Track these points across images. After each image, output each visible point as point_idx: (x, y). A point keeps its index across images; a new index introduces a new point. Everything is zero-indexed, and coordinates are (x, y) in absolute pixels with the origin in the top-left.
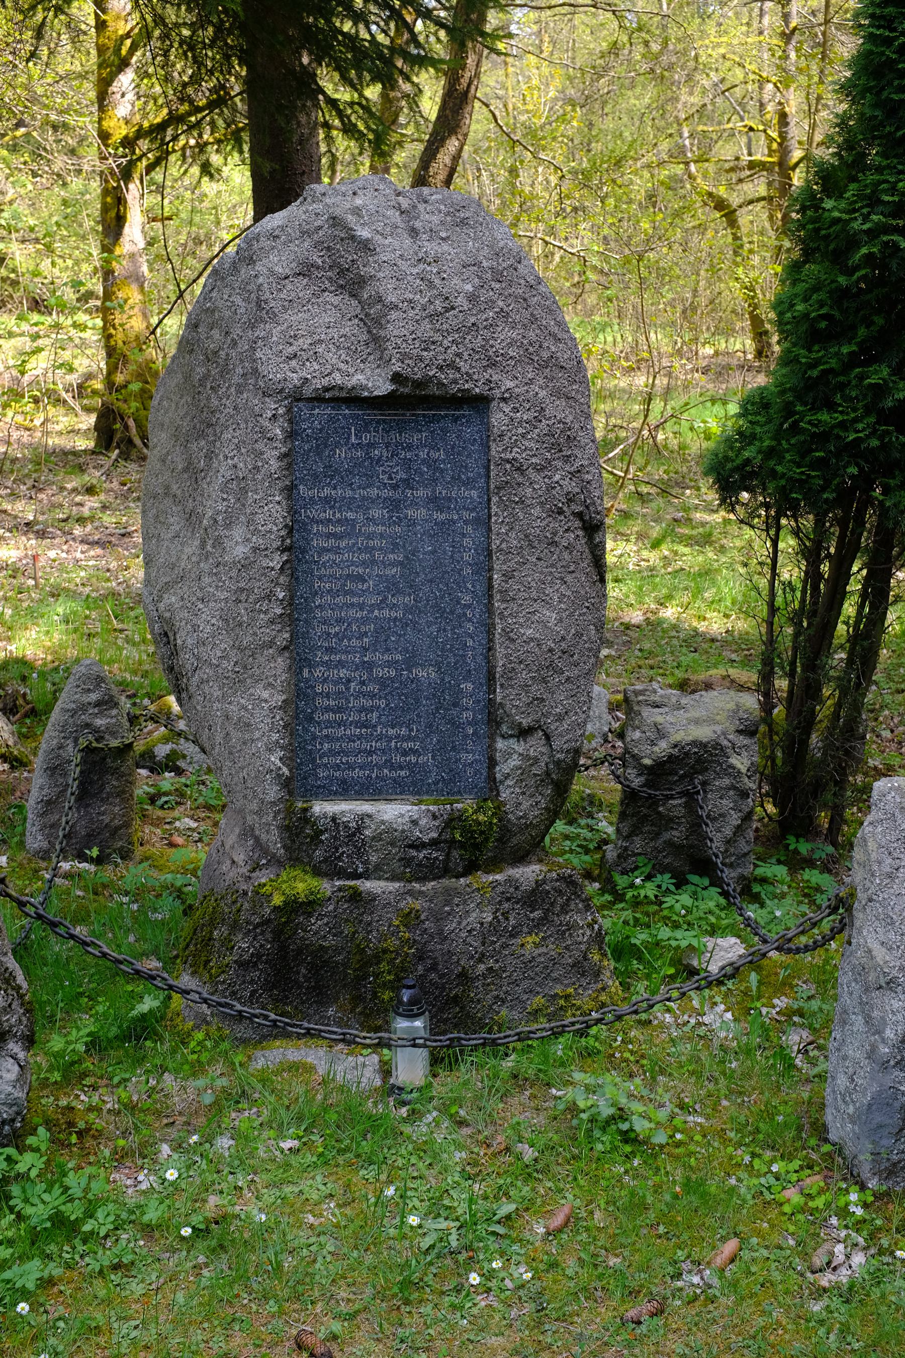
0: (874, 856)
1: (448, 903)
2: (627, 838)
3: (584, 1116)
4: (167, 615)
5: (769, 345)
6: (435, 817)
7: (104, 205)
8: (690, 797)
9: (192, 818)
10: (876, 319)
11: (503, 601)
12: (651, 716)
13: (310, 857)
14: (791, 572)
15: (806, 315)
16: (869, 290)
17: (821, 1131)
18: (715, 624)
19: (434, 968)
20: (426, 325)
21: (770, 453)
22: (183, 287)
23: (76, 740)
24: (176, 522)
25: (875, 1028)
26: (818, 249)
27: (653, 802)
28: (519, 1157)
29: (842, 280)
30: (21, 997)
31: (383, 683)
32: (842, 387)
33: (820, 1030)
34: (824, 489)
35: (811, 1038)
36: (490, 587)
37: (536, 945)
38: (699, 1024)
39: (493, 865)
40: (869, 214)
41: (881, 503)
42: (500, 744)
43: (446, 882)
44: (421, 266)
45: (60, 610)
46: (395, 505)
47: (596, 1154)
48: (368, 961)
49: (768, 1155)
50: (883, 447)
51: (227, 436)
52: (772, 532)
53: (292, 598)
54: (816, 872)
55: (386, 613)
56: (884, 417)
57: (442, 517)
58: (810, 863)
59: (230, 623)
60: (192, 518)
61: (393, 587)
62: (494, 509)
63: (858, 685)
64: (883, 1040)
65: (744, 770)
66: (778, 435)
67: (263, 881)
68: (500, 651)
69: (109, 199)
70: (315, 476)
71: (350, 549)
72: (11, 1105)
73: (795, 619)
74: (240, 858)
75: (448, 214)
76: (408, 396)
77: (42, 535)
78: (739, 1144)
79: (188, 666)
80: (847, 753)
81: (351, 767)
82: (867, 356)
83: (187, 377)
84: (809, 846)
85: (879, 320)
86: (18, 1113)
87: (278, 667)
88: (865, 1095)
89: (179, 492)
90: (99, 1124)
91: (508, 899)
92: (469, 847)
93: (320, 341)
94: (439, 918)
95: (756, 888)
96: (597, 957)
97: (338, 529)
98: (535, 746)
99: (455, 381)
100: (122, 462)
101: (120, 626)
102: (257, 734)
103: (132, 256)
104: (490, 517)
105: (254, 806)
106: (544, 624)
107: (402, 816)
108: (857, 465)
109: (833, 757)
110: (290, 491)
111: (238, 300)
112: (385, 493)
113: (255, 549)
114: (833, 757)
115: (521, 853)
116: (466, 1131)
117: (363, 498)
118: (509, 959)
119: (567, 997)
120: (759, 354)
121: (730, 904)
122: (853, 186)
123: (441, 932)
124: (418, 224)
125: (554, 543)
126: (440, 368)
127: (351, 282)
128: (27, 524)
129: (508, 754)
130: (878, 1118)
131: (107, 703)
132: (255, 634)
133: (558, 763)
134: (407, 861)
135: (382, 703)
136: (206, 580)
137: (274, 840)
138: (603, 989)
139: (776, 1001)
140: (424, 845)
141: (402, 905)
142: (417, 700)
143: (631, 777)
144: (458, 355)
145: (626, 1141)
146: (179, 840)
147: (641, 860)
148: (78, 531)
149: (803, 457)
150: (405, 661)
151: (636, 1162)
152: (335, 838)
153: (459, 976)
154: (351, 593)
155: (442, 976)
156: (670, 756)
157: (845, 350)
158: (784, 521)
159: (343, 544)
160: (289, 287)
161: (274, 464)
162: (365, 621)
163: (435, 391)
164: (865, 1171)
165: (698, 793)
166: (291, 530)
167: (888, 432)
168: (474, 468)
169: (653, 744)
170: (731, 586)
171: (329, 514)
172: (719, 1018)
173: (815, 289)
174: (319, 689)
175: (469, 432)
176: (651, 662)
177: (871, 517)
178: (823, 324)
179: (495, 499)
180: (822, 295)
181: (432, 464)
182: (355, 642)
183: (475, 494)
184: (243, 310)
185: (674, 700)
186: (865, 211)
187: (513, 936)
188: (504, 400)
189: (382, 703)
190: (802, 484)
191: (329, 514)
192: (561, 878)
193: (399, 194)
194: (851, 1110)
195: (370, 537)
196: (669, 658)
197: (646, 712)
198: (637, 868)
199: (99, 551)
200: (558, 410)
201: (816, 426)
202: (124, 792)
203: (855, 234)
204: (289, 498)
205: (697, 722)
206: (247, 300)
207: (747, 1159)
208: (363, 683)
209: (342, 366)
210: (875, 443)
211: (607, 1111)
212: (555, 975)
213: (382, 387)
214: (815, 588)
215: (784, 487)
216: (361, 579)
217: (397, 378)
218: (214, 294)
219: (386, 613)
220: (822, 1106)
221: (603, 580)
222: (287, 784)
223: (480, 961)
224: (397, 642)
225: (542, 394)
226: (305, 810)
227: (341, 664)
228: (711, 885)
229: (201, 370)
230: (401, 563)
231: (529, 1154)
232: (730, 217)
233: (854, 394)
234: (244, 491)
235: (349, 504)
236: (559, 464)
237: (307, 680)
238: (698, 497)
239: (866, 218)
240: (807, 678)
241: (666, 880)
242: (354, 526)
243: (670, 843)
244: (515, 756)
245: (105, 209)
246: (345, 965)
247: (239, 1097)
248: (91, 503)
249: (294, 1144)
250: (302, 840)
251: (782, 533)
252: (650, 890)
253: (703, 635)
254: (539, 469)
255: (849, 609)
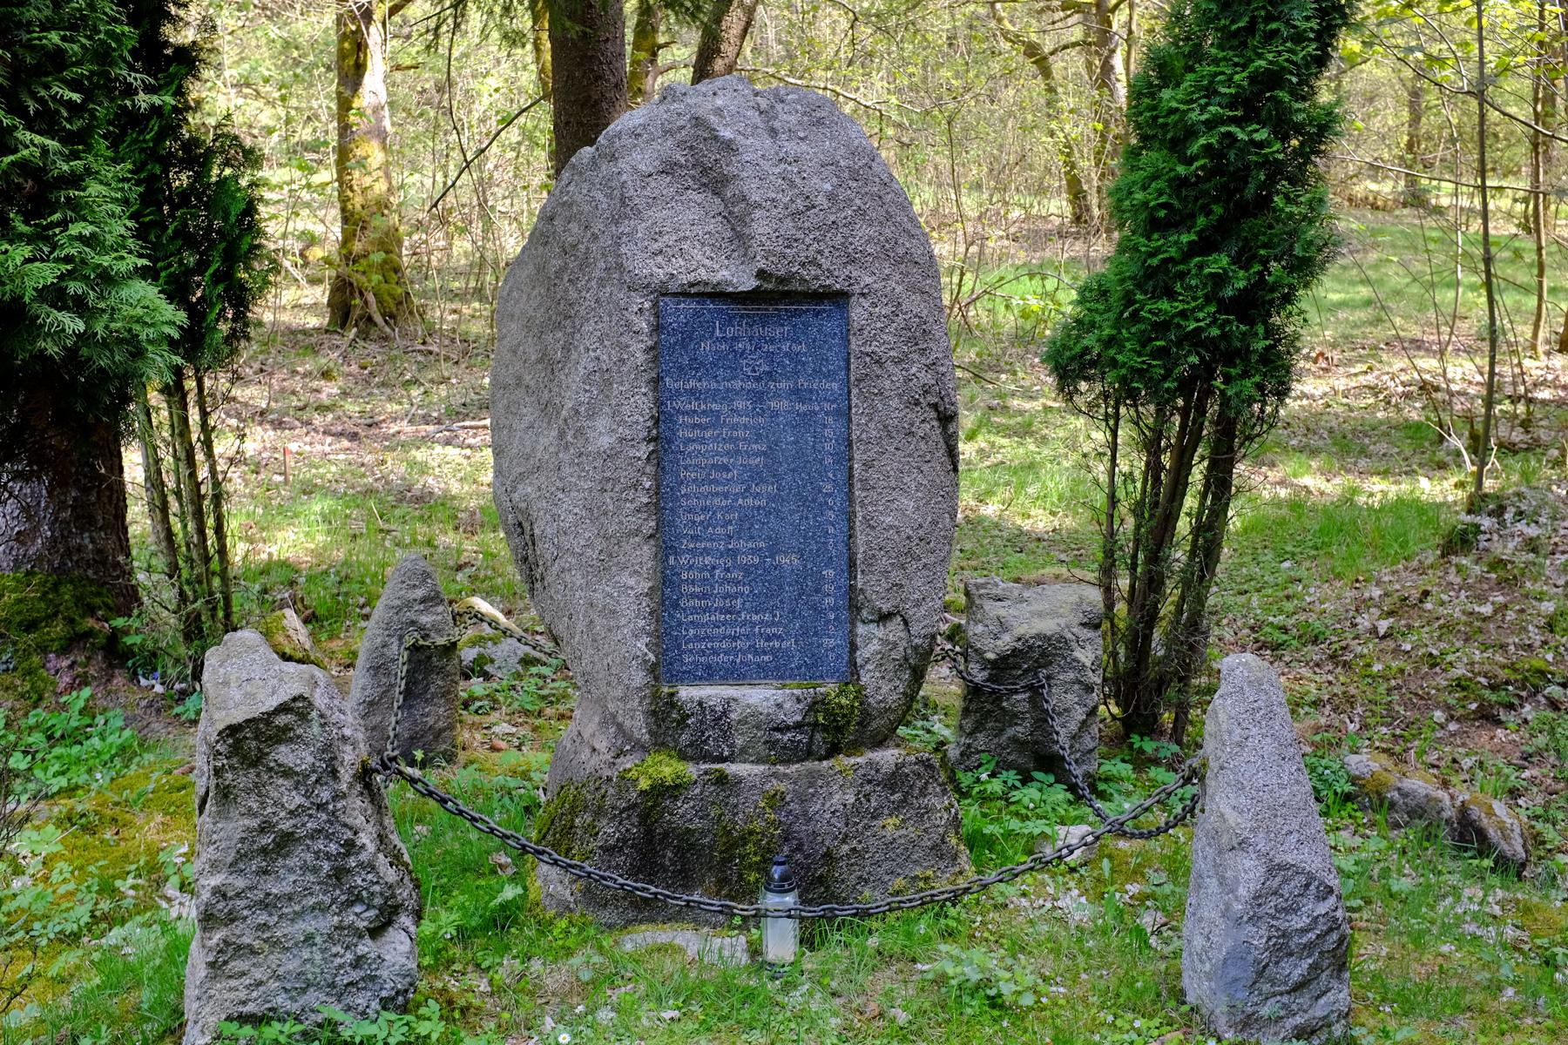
0: (1224, 726)
1: (811, 785)
2: (970, 735)
3: (954, 982)
4: (523, 505)
5: (1088, 209)
6: (799, 700)
7: (341, 51)
8: (1035, 691)
9: (509, 722)
10: (1214, 207)
11: (864, 490)
12: (993, 609)
13: (675, 741)
14: (1132, 462)
15: (1145, 204)
16: (1207, 179)
17: (1180, 996)
18: (1041, 521)
19: (799, 848)
20: (788, 223)
21: (1110, 342)
22: (469, 157)
23: (401, 638)
24: (529, 413)
25: (1228, 886)
26: (1155, 136)
27: (997, 697)
28: (893, 1020)
29: (1181, 170)
30: (410, 873)
31: (747, 570)
32: (1182, 276)
33: (1173, 914)
34: (1165, 378)
35: (1164, 920)
36: (851, 476)
37: (897, 828)
38: (1054, 908)
39: (854, 748)
40: (1207, 104)
41: (1223, 392)
42: (861, 629)
43: (809, 765)
44: (783, 166)
45: (317, 508)
46: (758, 397)
47: (965, 1018)
48: (733, 843)
49: (1130, 1016)
50: (1224, 336)
51: (586, 328)
52: (1111, 422)
53: (658, 487)
54: (1162, 770)
55: (750, 501)
56: (1224, 306)
57: (803, 408)
58: (1156, 762)
59: (594, 513)
60: (548, 409)
61: (756, 476)
62: (854, 401)
63: (1202, 578)
64: (1237, 899)
65: (1088, 664)
66: (1118, 323)
67: (628, 766)
68: (860, 539)
69: (346, 45)
70: (681, 369)
71: (715, 439)
72: (405, 976)
73: (1137, 510)
74: (602, 745)
75: (805, 114)
76: (772, 291)
77: (278, 425)
78: (1102, 1008)
79: (548, 556)
80: (1192, 647)
81: (716, 652)
82: (1206, 246)
83: (540, 269)
84: (1154, 745)
85: (1218, 210)
86: (411, 984)
87: (646, 553)
88: (1220, 951)
89: (532, 383)
90: (476, 1002)
91: (869, 782)
92: (833, 730)
93: (686, 238)
94: (803, 800)
95: (1102, 786)
96: (954, 841)
97: (703, 420)
98: (894, 630)
99: (816, 278)
100: (362, 343)
101: (386, 527)
102: (623, 621)
103: (377, 109)
104: (850, 408)
105: (619, 692)
106: (903, 512)
107: (767, 699)
108: (1198, 354)
109: (1177, 651)
110: (656, 382)
111: (600, 196)
112: (749, 385)
113: (621, 440)
114: (1177, 651)
115: (880, 737)
116: (838, 1001)
117: (728, 390)
118: (872, 840)
119: (926, 879)
120: (1077, 219)
121: (1079, 798)
122: (1190, 76)
123: (805, 813)
124: (777, 124)
125: (911, 433)
126: (803, 265)
127: (713, 181)
128: (262, 413)
129: (868, 639)
130: (1233, 972)
131: (432, 599)
132: (621, 522)
133: (915, 648)
134: (772, 744)
135: (747, 590)
136: (567, 470)
137: (639, 726)
138: (961, 873)
139: (1128, 887)
140: (788, 728)
141: (767, 787)
142: (781, 587)
143: (974, 672)
144: (820, 252)
145: (993, 1006)
146: (503, 745)
147: (985, 757)
148: (318, 420)
149: (1144, 345)
150: (770, 548)
151: (1005, 1024)
152: (702, 722)
153: (825, 856)
154: (716, 482)
155: (807, 857)
156: (1014, 650)
157: (1185, 238)
158: (1123, 410)
159: (708, 435)
160: (653, 184)
161: (641, 357)
162: (729, 509)
163: (796, 286)
164: (1222, 1023)
165: (1043, 687)
166: (657, 421)
167: (1228, 322)
168: (836, 363)
169: (996, 638)
170: (1056, 481)
171: (694, 405)
172: (1076, 905)
173: (1155, 177)
174: (684, 576)
175: (830, 326)
176: (974, 563)
177: (1213, 409)
178: (1162, 213)
179: (855, 391)
180: (1160, 184)
181: (794, 357)
182: (719, 530)
183: (835, 386)
184: (605, 206)
185: (1016, 593)
186: (1203, 101)
187: (874, 818)
188: (863, 295)
189: (747, 590)
190: (1140, 373)
191: (694, 405)
192: (919, 762)
193: (756, 94)
194: (1208, 967)
195: (734, 427)
196: (993, 559)
197: (988, 605)
198: (980, 765)
199: (345, 443)
200: (914, 304)
201: (1156, 315)
202: (449, 692)
203: (1193, 125)
204: (655, 389)
205: (1040, 615)
206: (610, 196)
207: (1110, 1018)
208: (727, 570)
209: (707, 262)
210: (1215, 332)
211: (975, 977)
212: (914, 857)
213: (748, 283)
214: (1157, 479)
215: (1124, 377)
216: (726, 468)
217: (761, 274)
218: (571, 188)
219: (750, 501)
220: (1179, 975)
221: (955, 470)
222: (653, 670)
223: (844, 841)
224: (761, 530)
225: (899, 289)
226: (672, 695)
227: (706, 552)
228: (1057, 781)
229: (557, 263)
230: (764, 453)
231: (902, 1017)
232: (1043, 66)
233: (1193, 283)
234: (609, 383)
235: (714, 395)
236: (915, 356)
237: (673, 568)
238: (1014, 381)
239: (1203, 109)
240: (1150, 571)
241: (1011, 776)
242: (718, 417)
243: (1014, 739)
244: (875, 641)
245: (342, 55)
246: (711, 847)
247: (608, 978)
248: (330, 390)
249: (676, 1014)
250: (668, 724)
251: (1121, 422)
252: (996, 786)
253: (1028, 533)
254: (897, 362)
255: (1190, 502)
